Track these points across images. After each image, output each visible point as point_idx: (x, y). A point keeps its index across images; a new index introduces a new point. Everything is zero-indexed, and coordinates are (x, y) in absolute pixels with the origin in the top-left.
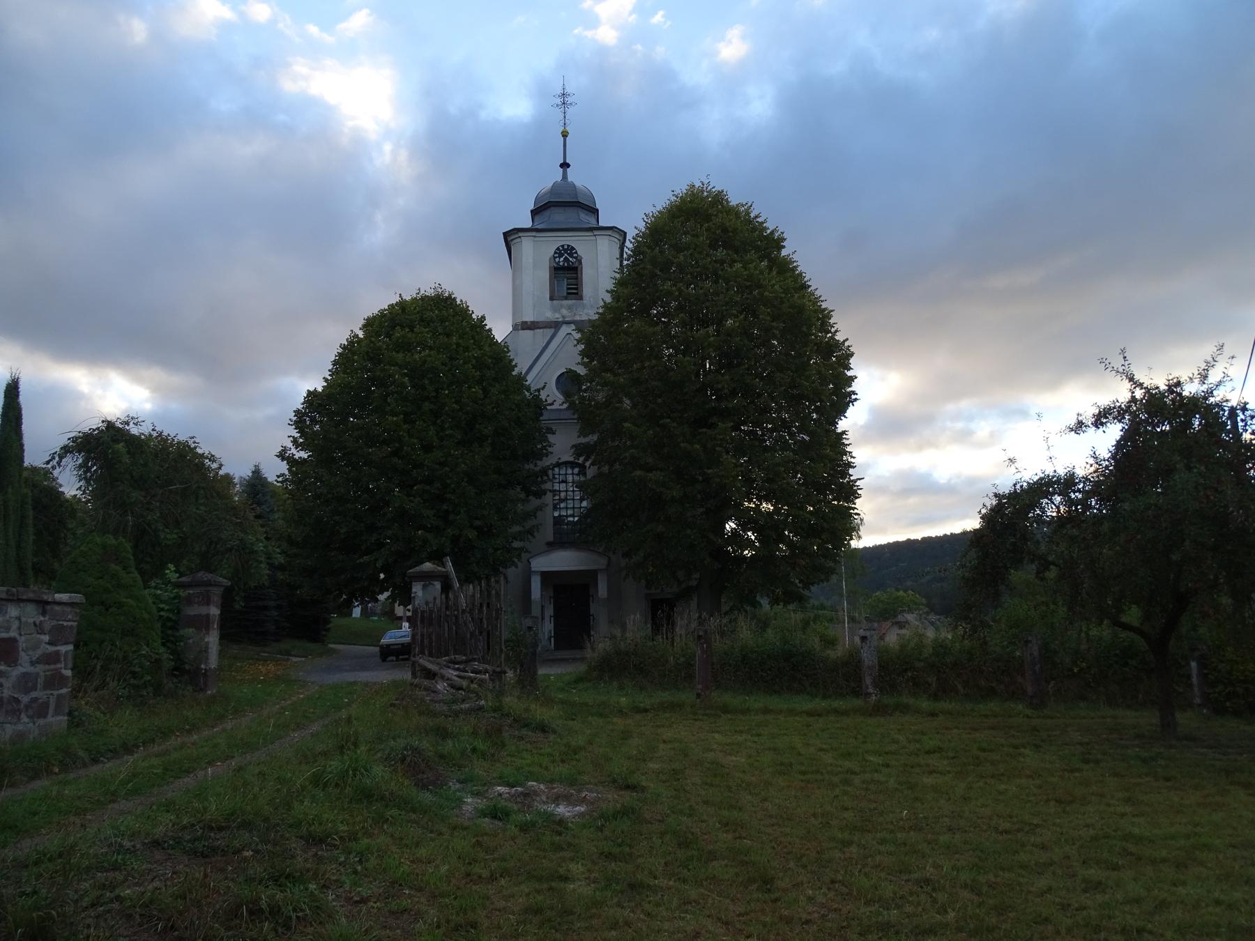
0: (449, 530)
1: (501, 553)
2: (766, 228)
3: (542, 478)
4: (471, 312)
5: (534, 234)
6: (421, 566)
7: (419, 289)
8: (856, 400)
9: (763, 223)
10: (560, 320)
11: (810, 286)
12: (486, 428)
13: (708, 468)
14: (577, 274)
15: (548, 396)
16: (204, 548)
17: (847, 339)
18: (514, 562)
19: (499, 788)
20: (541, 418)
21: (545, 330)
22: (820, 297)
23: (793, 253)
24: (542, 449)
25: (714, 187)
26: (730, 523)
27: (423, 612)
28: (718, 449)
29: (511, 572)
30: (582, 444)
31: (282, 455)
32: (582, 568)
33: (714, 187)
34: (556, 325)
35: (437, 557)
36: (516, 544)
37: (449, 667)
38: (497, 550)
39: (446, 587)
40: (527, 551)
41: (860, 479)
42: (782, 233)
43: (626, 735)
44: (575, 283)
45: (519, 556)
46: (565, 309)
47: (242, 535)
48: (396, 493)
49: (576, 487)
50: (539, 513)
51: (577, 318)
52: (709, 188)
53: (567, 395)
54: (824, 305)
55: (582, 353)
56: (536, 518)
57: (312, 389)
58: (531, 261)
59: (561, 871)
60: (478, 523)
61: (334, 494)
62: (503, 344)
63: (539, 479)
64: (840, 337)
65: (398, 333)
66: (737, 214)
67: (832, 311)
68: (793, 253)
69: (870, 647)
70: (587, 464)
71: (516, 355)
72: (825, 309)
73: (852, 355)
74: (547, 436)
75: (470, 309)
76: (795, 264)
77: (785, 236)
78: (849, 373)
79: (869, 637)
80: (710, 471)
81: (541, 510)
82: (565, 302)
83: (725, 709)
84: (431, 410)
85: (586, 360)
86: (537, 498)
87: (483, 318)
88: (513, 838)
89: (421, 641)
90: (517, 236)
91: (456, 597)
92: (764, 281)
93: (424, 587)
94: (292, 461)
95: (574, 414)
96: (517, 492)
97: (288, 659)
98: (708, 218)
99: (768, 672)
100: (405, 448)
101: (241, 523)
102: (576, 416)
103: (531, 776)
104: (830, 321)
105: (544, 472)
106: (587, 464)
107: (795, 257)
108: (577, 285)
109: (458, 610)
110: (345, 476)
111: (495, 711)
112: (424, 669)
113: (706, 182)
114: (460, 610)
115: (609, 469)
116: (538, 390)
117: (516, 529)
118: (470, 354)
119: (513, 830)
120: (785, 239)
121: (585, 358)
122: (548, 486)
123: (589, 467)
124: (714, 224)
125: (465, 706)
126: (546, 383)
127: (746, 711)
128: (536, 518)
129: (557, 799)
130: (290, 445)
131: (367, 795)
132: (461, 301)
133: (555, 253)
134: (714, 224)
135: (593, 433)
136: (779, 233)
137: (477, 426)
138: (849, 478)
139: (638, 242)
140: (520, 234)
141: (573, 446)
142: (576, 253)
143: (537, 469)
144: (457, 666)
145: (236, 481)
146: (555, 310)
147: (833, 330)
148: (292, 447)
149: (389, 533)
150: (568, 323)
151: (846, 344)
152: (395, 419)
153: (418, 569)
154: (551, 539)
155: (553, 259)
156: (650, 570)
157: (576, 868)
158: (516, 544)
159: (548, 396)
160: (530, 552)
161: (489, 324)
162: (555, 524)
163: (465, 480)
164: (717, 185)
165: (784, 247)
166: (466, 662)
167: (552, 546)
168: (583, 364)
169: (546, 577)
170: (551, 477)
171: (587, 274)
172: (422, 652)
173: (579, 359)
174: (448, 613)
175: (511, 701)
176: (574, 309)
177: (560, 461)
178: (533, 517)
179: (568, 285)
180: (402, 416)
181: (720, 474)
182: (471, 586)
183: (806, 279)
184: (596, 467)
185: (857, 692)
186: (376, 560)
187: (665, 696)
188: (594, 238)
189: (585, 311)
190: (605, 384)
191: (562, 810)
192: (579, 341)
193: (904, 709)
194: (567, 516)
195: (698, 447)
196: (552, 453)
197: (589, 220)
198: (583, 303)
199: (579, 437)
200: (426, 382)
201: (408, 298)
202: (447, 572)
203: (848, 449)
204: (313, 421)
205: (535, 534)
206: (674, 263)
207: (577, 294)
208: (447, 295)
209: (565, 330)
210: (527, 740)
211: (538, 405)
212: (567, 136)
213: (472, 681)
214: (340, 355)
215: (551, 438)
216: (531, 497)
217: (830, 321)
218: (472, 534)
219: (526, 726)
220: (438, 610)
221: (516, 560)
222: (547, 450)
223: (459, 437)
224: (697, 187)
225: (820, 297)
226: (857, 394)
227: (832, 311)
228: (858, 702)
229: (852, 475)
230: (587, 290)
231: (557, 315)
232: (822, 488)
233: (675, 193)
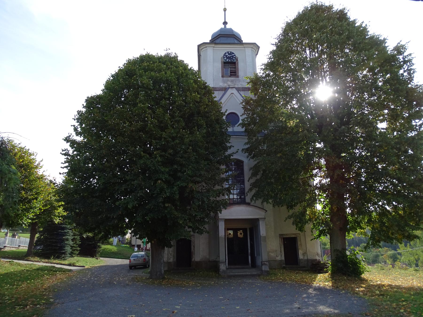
10: (227, 87)
21: (220, 92)
51: (236, 86)
142: (235, 55)
146: (224, 82)
169: (227, 221)
230: (241, 73)
231: (225, 85)
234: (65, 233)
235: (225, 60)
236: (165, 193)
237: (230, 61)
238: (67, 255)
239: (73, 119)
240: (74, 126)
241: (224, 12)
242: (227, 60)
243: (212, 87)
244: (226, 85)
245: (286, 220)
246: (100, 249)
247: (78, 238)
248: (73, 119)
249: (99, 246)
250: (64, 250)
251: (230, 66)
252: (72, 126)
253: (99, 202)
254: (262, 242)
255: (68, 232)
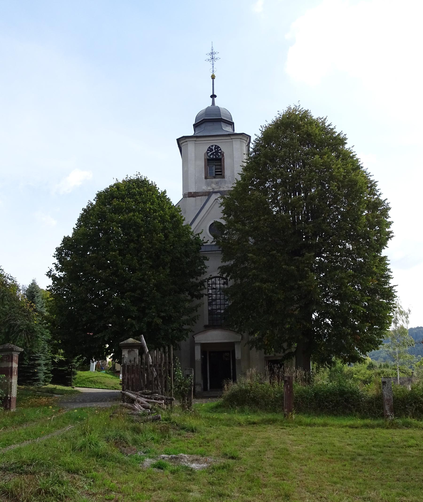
0: (146, 319)
1: (176, 332)
2: (335, 132)
3: (201, 287)
4: (157, 189)
5: (195, 139)
6: (127, 340)
7: (127, 176)
8: (392, 236)
9: (333, 129)
10: (211, 191)
11: (362, 167)
12: (166, 258)
13: (300, 281)
14: (221, 162)
15: (204, 237)
16: (7, 330)
17: (386, 199)
18: (184, 337)
19: (163, 455)
20: (200, 251)
21: (202, 197)
22: (369, 173)
23: (353, 147)
24: (200, 270)
25: (302, 108)
26: (315, 314)
27: (128, 366)
28: (306, 269)
29: (183, 344)
30: (225, 266)
31: (49, 274)
32: (226, 341)
33: (302, 108)
34: (209, 194)
35: (136, 335)
36: (185, 327)
37: (142, 397)
38: (173, 330)
39: (142, 352)
40: (192, 331)
41: (395, 286)
42: (345, 135)
43: (239, 435)
44: (220, 168)
45: (187, 334)
46: (214, 184)
47: (28, 322)
48: (115, 297)
49: (222, 292)
50: (198, 309)
51: (222, 189)
52: (300, 109)
53: (215, 237)
54: (372, 178)
55: (224, 212)
56: (197, 312)
57: (66, 236)
58: (193, 155)
59: (187, 488)
60: (163, 314)
61: (79, 297)
62: (177, 207)
63: (199, 288)
64: (382, 198)
65: (115, 202)
66: (317, 125)
67: (377, 182)
68: (353, 147)
69: (388, 388)
70: (229, 278)
71: (185, 213)
72: (372, 181)
73: (390, 209)
74: (203, 262)
75: (157, 186)
76: (354, 154)
77: (347, 136)
78: (389, 220)
79: (387, 382)
80: (300, 283)
81: (200, 306)
82: (214, 180)
83: (300, 423)
84: (135, 248)
85: (226, 216)
86: (198, 299)
87: (165, 192)
88: (167, 476)
89: (127, 382)
90: (185, 141)
91: (147, 357)
92: (333, 165)
93: (129, 352)
94: (54, 278)
95: (220, 248)
96: (186, 295)
97: (53, 395)
98: (298, 127)
99: (331, 403)
100: (120, 270)
101: (27, 315)
102: (221, 249)
103: (180, 451)
104: (376, 188)
105: (202, 283)
106: (229, 278)
107: (353, 150)
108: (221, 169)
109: (147, 365)
110: (86, 287)
111: (166, 420)
112: (129, 397)
113: (298, 105)
114: (149, 365)
115: (241, 282)
116: (198, 234)
117: (185, 318)
118: (157, 214)
119: (167, 472)
120: (347, 139)
121: (225, 215)
122: (205, 292)
123: (230, 280)
124: (302, 132)
125: (150, 417)
126: (202, 230)
127: (314, 425)
128: (197, 312)
129: (192, 462)
130: (54, 268)
131: (98, 456)
132: (152, 182)
133: (208, 150)
134: (302, 132)
135: (230, 259)
136: (343, 135)
137: (162, 257)
138: (389, 285)
139: (257, 143)
140: (187, 140)
141: (219, 268)
142: (220, 150)
143: (198, 282)
144: (146, 396)
145: (20, 288)
146: (208, 185)
147: (378, 193)
148: (55, 270)
149: (111, 320)
150: (216, 192)
151: (386, 202)
152: (114, 253)
153: (125, 342)
154: (207, 323)
155: (206, 154)
156: (266, 343)
157: (194, 487)
158: (185, 327)
159: (204, 237)
160: (194, 332)
161: (169, 195)
162: (209, 314)
163: (155, 289)
164: (304, 106)
165: (346, 143)
166: (151, 394)
167: (207, 328)
168: (223, 218)
169: (204, 346)
170: (206, 286)
171: (227, 162)
172: (128, 389)
173: (222, 215)
174: (142, 366)
175: (176, 416)
176: (220, 183)
177: (211, 277)
178: (195, 311)
179: (216, 169)
180: (118, 252)
181: (307, 284)
182: (155, 351)
183: (360, 163)
184: (233, 280)
185: (383, 416)
186: (105, 336)
187: (270, 416)
188: (231, 140)
189: (226, 185)
190: (237, 230)
191: (194, 465)
192: (222, 204)
193: (408, 425)
194: (217, 310)
195: (294, 268)
196: (206, 272)
197: (228, 129)
198: (225, 180)
199: (222, 262)
200: (132, 231)
201: (120, 181)
202: (141, 343)
203: (389, 267)
204: (67, 255)
205: (197, 321)
206: (278, 156)
207: (221, 174)
208: (143, 178)
209: (214, 197)
210: (183, 436)
211: (198, 243)
212: (214, 78)
213: (154, 403)
214: (82, 215)
215: (206, 263)
216: (194, 299)
217: (376, 188)
218: (159, 321)
219: (183, 428)
220: (136, 365)
221: (185, 336)
222: (204, 270)
223: (151, 263)
224: (292, 108)
225: (369, 173)
226: (393, 233)
227: (377, 182)
228: (381, 421)
229: (390, 284)
230: (227, 172)
231: (209, 188)
232: (374, 292)
233: (279, 113)
234: (37, 357)
235: (209, 157)
236: (135, 328)
237: (214, 157)
238: (40, 382)
239: (53, 256)
240: (54, 263)
241: (212, 80)
242: (212, 156)
243: (194, 192)
244: (209, 189)
245: (245, 345)
246: (76, 376)
247: (50, 363)
248: (53, 256)
249: (74, 372)
250: (38, 376)
251: (215, 164)
252: (53, 264)
253: (83, 335)
254: (236, 365)
255: (40, 357)
